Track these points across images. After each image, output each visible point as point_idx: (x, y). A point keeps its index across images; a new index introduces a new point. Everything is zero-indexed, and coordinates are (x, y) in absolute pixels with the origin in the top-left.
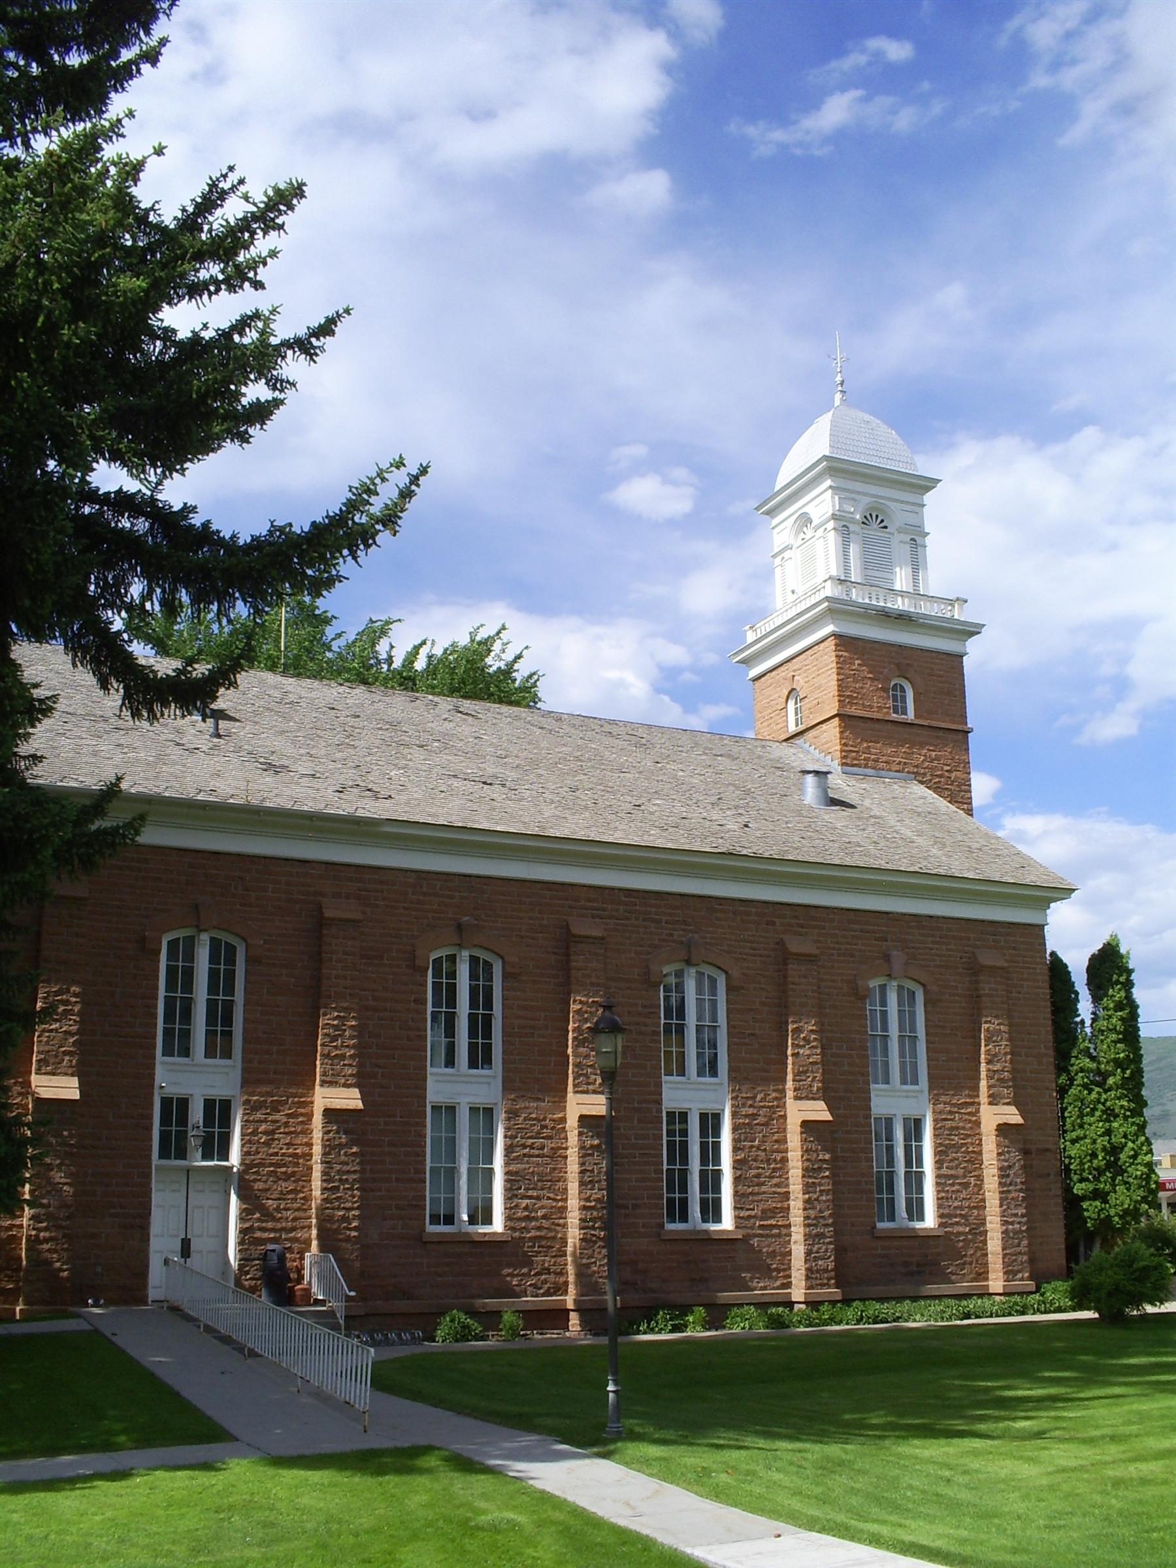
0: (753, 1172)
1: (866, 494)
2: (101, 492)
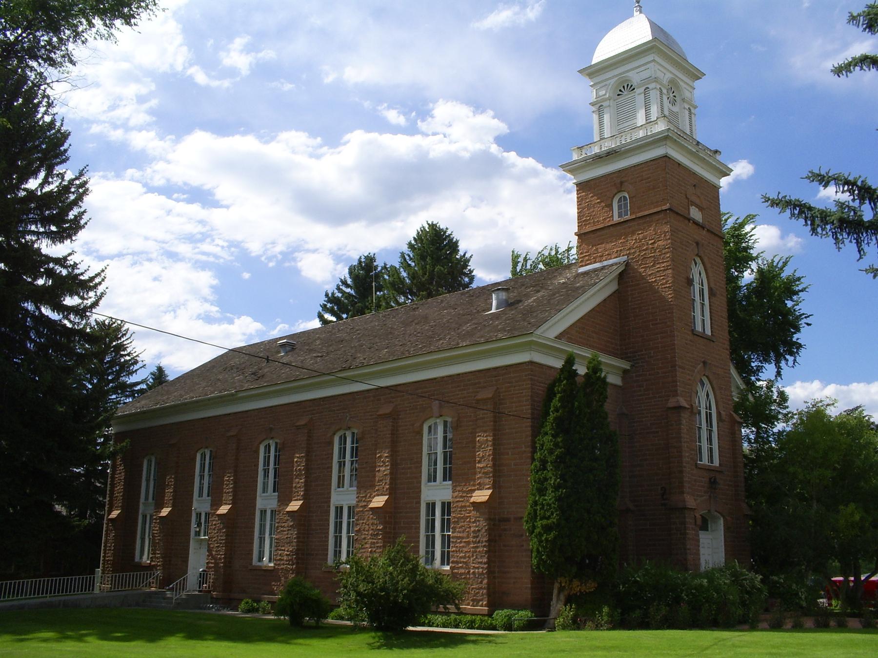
2: (215, 282)
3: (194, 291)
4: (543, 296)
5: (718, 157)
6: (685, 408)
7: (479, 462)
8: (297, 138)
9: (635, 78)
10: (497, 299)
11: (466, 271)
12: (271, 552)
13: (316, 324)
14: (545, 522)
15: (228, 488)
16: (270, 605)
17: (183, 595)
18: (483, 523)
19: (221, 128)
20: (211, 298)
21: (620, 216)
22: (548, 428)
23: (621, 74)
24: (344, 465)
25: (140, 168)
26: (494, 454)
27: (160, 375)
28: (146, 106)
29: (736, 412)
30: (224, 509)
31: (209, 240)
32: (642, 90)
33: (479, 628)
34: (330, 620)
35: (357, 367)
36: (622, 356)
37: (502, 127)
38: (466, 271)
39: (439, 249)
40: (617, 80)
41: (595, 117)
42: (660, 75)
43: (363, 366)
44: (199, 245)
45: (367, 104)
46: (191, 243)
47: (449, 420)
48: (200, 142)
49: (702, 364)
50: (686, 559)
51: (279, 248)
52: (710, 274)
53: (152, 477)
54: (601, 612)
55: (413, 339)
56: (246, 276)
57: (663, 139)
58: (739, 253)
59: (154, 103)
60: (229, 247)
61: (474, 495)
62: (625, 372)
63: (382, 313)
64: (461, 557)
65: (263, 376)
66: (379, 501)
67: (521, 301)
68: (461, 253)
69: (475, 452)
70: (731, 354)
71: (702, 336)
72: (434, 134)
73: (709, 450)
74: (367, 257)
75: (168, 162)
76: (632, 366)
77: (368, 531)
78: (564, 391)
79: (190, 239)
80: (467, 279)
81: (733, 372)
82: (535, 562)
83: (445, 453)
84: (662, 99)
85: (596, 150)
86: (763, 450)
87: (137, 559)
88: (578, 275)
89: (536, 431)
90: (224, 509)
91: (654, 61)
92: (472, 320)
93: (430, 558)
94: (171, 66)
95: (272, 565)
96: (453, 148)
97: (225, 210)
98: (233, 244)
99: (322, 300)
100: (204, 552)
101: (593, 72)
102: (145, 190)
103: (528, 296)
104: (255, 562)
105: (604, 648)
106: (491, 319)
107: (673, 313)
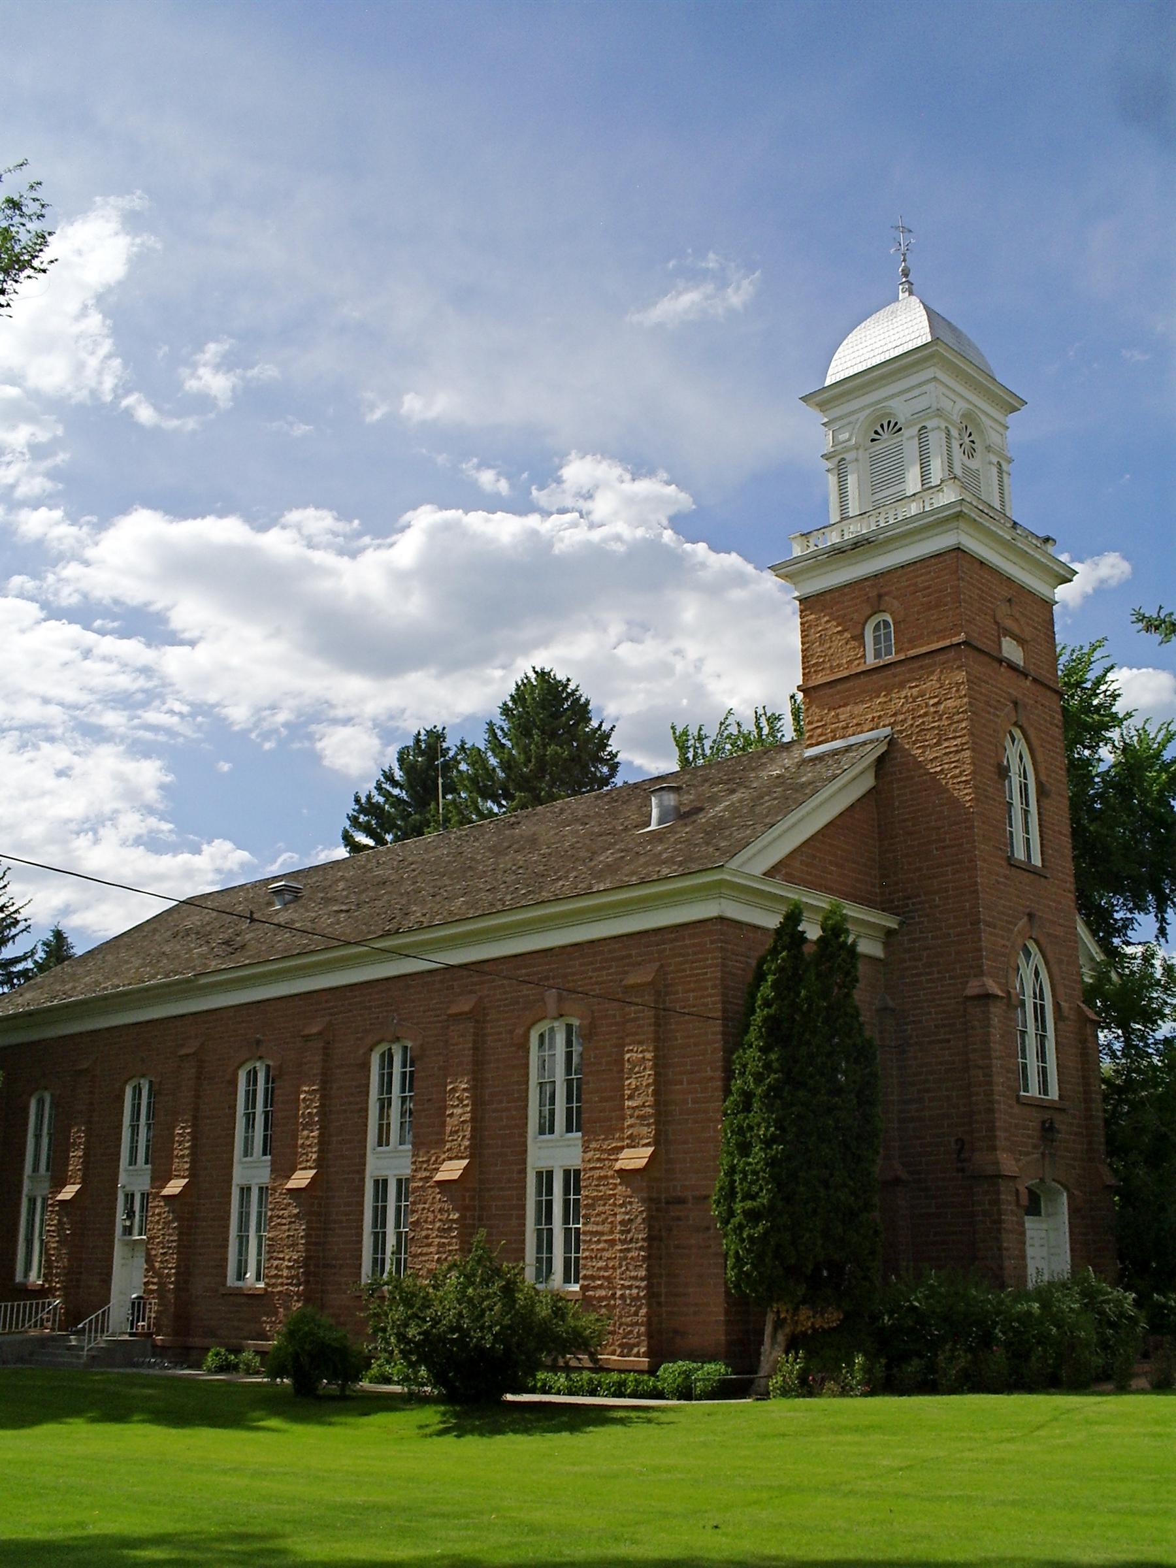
0: (424, 1233)
1: (862, 409)
3: (131, 794)
4: (741, 801)
5: (1050, 548)
6: (997, 997)
7: (631, 1097)
8: (317, 520)
9: (902, 410)
10: (660, 806)
11: (603, 754)
12: (259, 1262)
13: (342, 853)
14: (749, 1204)
15: (182, 1149)
16: (258, 1359)
17: (102, 1340)
18: (637, 1207)
19: (179, 506)
20: (161, 807)
21: (877, 655)
22: (752, 1035)
23: (879, 402)
24: (390, 1105)
25: (36, 575)
26: (656, 1082)
27: (58, 946)
28: (48, 463)
29: (1090, 1002)
30: (174, 1187)
31: (157, 703)
32: (914, 431)
33: (631, 1396)
34: (365, 1384)
35: (410, 930)
36: (886, 907)
37: (681, 499)
38: (603, 754)
39: (556, 715)
40: (871, 411)
41: (832, 480)
42: (947, 405)
43: (421, 928)
44: (139, 712)
45: (441, 459)
46: (125, 709)
47: (576, 1022)
48: (140, 529)
49: (1025, 919)
50: (1001, 1268)
51: (282, 717)
52: (1040, 758)
53: (45, 1131)
54: (850, 1364)
55: (510, 878)
56: (225, 767)
57: (955, 517)
58: (1088, 719)
59: (62, 458)
60: (193, 715)
61: (621, 1156)
62: (889, 933)
63: (455, 833)
64: (599, 1269)
65: (243, 947)
66: (452, 1170)
67: (701, 809)
68: (594, 724)
69: (622, 1080)
70: (1078, 898)
71: (1026, 868)
72: (562, 511)
73: (1041, 1072)
74: (429, 733)
75: (87, 563)
76: (901, 924)
77: (433, 1222)
78: (781, 969)
79: (122, 701)
80: (605, 770)
81: (1082, 930)
82: (731, 1274)
83: (569, 1083)
84: (949, 447)
85: (834, 538)
86: (1138, 1070)
87: (19, 1278)
88: (805, 761)
89: (734, 1040)
90: (174, 1187)
91: (935, 379)
92: (615, 843)
93: (544, 1269)
94: (94, 393)
95: (261, 1285)
96: (596, 535)
97: (187, 649)
98: (199, 709)
99: (351, 807)
100: (140, 1263)
101: (828, 399)
102: (42, 615)
103: (714, 800)
104: (231, 1281)
105: (856, 1429)
106: (649, 842)
107: (972, 827)
